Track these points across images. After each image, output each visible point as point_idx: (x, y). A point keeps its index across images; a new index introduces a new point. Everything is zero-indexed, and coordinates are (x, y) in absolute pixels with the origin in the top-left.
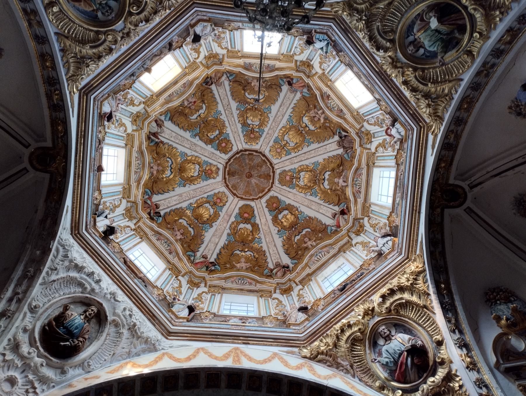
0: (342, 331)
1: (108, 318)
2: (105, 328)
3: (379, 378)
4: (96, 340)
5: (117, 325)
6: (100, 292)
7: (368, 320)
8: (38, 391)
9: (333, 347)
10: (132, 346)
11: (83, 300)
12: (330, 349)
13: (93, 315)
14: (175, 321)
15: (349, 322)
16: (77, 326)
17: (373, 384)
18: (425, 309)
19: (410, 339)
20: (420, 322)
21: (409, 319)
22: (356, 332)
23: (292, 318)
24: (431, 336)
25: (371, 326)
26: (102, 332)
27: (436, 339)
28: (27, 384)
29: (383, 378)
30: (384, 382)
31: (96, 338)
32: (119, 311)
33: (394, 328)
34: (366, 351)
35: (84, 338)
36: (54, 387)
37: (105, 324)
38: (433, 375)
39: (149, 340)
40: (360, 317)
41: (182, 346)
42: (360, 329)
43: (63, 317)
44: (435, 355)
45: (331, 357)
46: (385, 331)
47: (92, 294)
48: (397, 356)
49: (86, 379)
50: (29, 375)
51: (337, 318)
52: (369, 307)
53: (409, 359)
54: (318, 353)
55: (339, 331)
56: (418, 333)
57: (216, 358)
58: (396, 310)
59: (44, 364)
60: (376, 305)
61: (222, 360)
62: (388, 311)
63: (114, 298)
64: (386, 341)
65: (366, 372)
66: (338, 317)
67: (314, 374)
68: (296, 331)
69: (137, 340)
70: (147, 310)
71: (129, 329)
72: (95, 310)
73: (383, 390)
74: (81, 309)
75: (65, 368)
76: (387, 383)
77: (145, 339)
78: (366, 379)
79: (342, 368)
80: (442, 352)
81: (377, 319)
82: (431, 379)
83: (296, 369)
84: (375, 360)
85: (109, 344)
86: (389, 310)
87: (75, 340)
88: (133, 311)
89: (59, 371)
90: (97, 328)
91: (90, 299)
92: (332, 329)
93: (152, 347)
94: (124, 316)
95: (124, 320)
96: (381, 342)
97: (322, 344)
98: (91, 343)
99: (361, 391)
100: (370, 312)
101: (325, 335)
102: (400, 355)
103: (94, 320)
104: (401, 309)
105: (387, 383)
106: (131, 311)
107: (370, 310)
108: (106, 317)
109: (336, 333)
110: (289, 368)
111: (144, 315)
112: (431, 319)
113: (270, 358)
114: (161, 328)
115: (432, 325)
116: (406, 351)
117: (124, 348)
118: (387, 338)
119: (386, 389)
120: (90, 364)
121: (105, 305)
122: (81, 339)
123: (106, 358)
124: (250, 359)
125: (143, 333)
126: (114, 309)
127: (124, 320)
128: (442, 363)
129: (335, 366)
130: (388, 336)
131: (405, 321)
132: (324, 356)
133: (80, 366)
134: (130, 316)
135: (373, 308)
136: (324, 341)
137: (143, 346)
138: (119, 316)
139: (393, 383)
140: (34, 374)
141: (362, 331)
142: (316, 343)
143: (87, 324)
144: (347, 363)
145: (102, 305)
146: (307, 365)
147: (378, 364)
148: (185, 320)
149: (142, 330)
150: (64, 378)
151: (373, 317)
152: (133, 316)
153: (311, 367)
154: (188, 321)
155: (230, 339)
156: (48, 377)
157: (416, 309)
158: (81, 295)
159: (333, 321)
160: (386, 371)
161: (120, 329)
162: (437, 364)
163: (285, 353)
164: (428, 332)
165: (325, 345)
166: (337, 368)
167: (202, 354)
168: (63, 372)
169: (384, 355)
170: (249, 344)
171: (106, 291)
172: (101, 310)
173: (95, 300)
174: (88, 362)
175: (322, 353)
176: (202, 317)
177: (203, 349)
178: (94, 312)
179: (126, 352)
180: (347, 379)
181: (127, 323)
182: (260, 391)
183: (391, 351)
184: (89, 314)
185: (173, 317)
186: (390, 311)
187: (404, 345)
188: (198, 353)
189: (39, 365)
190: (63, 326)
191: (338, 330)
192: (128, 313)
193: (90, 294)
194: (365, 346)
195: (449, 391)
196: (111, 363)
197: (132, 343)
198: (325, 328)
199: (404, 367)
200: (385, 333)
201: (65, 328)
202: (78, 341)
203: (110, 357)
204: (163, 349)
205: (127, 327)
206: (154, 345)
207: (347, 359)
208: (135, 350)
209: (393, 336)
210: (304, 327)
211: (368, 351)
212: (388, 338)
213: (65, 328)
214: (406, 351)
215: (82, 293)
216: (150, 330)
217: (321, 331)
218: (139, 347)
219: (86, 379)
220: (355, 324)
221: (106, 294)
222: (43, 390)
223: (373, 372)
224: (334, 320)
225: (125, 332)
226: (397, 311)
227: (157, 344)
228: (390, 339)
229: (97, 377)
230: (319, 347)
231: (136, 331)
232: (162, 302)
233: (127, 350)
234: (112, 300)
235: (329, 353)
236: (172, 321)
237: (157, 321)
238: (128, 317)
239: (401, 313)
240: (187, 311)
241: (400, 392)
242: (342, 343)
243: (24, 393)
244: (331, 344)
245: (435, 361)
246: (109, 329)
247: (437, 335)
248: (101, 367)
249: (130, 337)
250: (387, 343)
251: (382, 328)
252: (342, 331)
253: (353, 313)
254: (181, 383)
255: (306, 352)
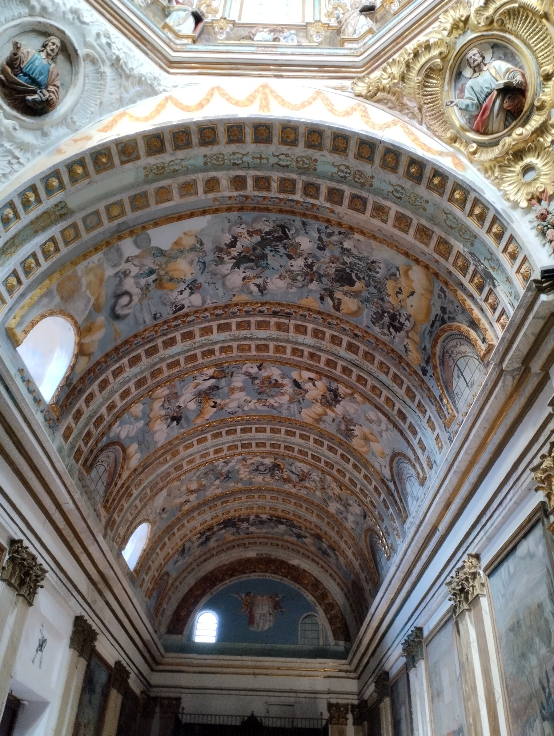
0: (416, 55)
1: (79, 52)
2: (78, 67)
3: (453, 126)
4: (72, 87)
5: (94, 61)
6: (56, 10)
7: (456, 38)
8: (21, 160)
9: (399, 81)
10: (122, 89)
11: (37, 28)
12: (394, 84)
13: (56, 50)
14: (175, 44)
15: (428, 41)
16: (40, 71)
17: (443, 134)
18: (544, 20)
19: (508, 70)
20: (531, 42)
21: (517, 36)
22: (434, 58)
23: (349, 26)
24: (540, 65)
25: (458, 47)
26: (77, 73)
27: (544, 70)
28: (6, 154)
29: (458, 126)
30: (458, 132)
31: (72, 82)
32: (91, 39)
33: (491, 51)
34: (443, 87)
35: (55, 85)
36: (39, 153)
37: (78, 62)
38: (523, 125)
39: (143, 79)
40: (446, 33)
41: (190, 84)
42: (441, 53)
43: (17, 59)
44: (536, 95)
45: (394, 94)
46: (476, 58)
47: (45, 15)
48: (483, 96)
49: (75, 141)
50: (3, 143)
51: (413, 31)
52: (462, 16)
53: (498, 102)
54: (378, 90)
55: (412, 56)
56: (523, 60)
57: (237, 103)
58: (500, 21)
59: (17, 127)
60: (473, 10)
61: (245, 106)
62: (488, 22)
63: (79, 18)
64: (475, 72)
65: (438, 117)
66: (416, 28)
67: (367, 123)
68: (352, 51)
69: (128, 81)
70: (131, 29)
71: (112, 65)
72: (57, 42)
73: (455, 142)
74: (38, 42)
75: (46, 129)
76: (462, 133)
77: (137, 78)
78: (436, 127)
79: (407, 111)
80: (546, 90)
81: (470, 36)
82: (519, 130)
83: (344, 116)
84: (452, 102)
85: (91, 90)
86: (491, 22)
87: (44, 91)
88: (112, 37)
89: (39, 133)
90: (68, 66)
91: (46, 25)
92: (402, 51)
93: (150, 89)
94: (100, 46)
95: (101, 52)
96: (467, 72)
97: (385, 76)
98: (67, 92)
99: (425, 145)
100: (461, 24)
101: (391, 60)
102: (489, 94)
103: (61, 58)
104: (510, 18)
105: (462, 133)
106: (107, 36)
107: (462, 21)
108: (76, 51)
109: (406, 57)
110: (334, 114)
111: (129, 38)
112: (549, 37)
113: (310, 100)
114: (157, 56)
115: (546, 48)
116: (497, 90)
117: (111, 94)
118: (477, 69)
119: (458, 141)
120: (74, 120)
121: (68, 32)
122: (52, 88)
123: (93, 109)
124: (283, 103)
125: (133, 69)
126: (84, 36)
127: (101, 52)
128: (540, 108)
129: (398, 108)
130: (479, 65)
131: (509, 40)
132: (385, 94)
133: (62, 123)
134: (109, 45)
135: (468, 18)
136: (389, 70)
137: (138, 88)
138: (93, 48)
139: (468, 134)
140: (10, 141)
141: (443, 55)
142: (377, 74)
143: (53, 65)
144: (415, 105)
145: (63, 32)
146: (360, 108)
147: (455, 108)
148: (190, 41)
149: (130, 66)
150: (48, 142)
151: (464, 32)
152: (113, 45)
153: (365, 111)
154: (194, 42)
155: (255, 70)
156: (28, 143)
157: (531, 19)
158: (29, 19)
159: (406, 36)
160: (464, 117)
161: (100, 67)
162: (535, 108)
163: (333, 90)
164: (537, 58)
165: (389, 77)
166: (401, 111)
167: (217, 95)
168: (45, 134)
169: (467, 94)
170: (282, 76)
171: (63, 9)
172: (65, 41)
173: (51, 25)
174: (72, 118)
175: (384, 89)
176: (216, 29)
177: (218, 88)
178: (57, 46)
179: (117, 99)
180: (410, 127)
181: (107, 57)
182: (297, 146)
183: (477, 89)
184: (51, 50)
185: (171, 35)
186: (492, 22)
187: (497, 81)
188: (212, 95)
189: (11, 129)
190: (22, 72)
191: (410, 54)
192: (104, 40)
193: (43, 17)
194: (444, 79)
195: (536, 148)
196: (101, 114)
197: (120, 85)
198: (394, 47)
199: (488, 113)
200: (475, 61)
201: (25, 74)
202: (48, 91)
203: (97, 108)
204: (164, 90)
205: (108, 63)
206: (151, 85)
207: (415, 98)
208: (127, 95)
209: (485, 65)
210: (365, 44)
211: (446, 88)
212: (477, 69)
213: (25, 74)
214: (497, 90)
215: (30, 15)
216: (142, 64)
217: (388, 51)
218: (134, 90)
219: (75, 141)
220: (436, 44)
221: (64, 13)
222: (28, 159)
223: (448, 117)
224: (409, 33)
225: (107, 70)
226: (503, 22)
227: (155, 84)
228: (481, 70)
229: (89, 138)
230: (379, 80)
231: (122, 67)
232: (153, 7)
233: (117, 96)
234: (77, 22)
235: (394, 89)
236: (172, 44)
237: (149, 47)
238: (106, 48)
239: (507, 26)
240: (191, 21)
241: (475, 146)
242: (413, 74)
243: (7, 165)
244: (397, 76)
245: (532, 105)
246: (85, 68)
247: (548, 65)
248: (90, 122)
249: (116, 78)
250: (476, 75)
251: (473, 54)
252: (416, 55)
253: (436, 24)
254: (195, 139)
255: (362, 88)
